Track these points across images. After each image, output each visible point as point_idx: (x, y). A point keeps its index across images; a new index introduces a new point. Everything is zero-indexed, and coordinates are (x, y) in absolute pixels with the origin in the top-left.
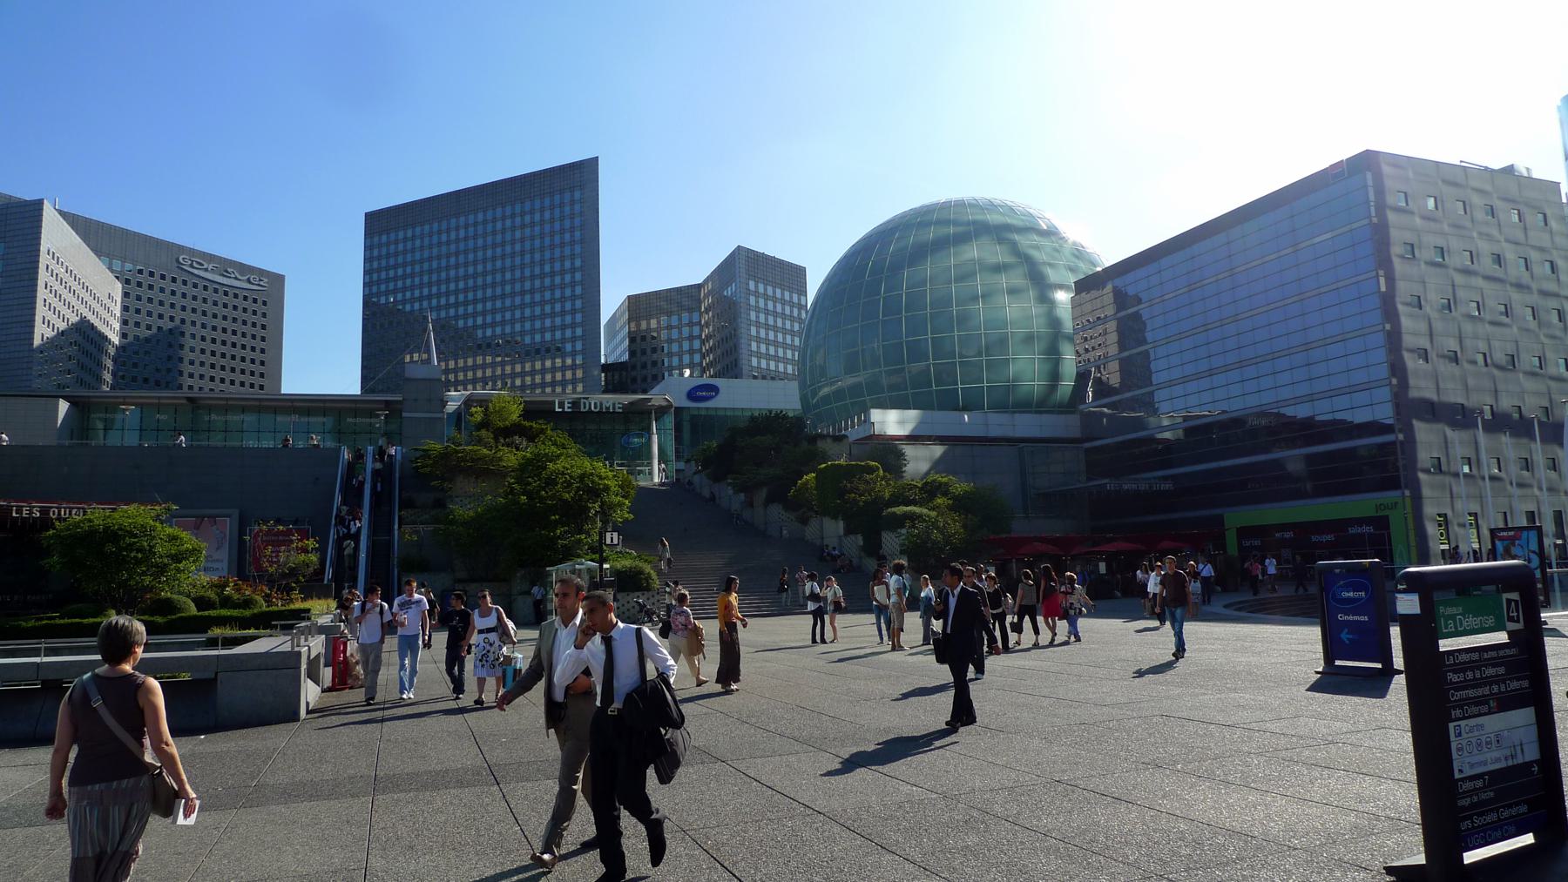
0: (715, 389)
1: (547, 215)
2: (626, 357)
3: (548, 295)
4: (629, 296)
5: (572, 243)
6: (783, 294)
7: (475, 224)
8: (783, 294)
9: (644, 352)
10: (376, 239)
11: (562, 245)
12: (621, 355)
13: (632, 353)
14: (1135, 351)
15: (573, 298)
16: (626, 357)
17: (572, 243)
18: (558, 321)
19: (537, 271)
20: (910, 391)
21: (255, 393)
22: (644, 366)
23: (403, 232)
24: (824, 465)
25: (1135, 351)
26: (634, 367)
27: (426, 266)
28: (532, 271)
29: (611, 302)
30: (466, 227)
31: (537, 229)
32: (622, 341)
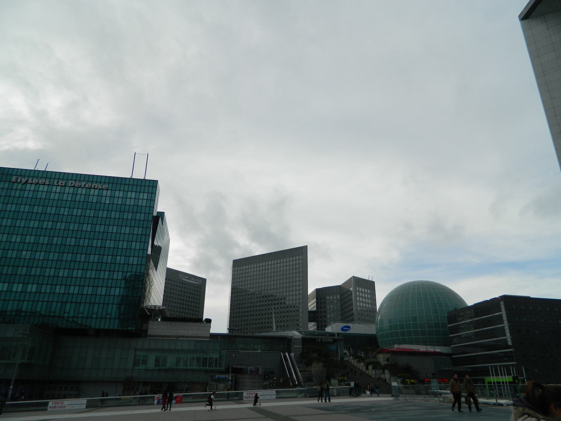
0: (349, 327)
1: (291, 263)
2: (315, 309)
3: (285, 290)
4: (317, 289)
5: (299, 272)
6: (367, 291)
7: (296, 260)
8: (367, 291)
9: (321, 308)
10: (236, 269)
11: (296, 273)
12: (313, 308)
13: (317, 308)
14: (462, 333)
15: (299, 290)
16: (315, 309)
17: (299, 272)
18: (298, 297)
19: (288, 281)
20: (433, 322)
21: (196, 317)
22: (321, 312)
23: (270, 262)
24: (296, 382)
25: (462, 333)
26: (318, 313)
27: (252, 278)
28: (299, 279)
29: (311, 289)
30: (293, 261)
31: (288, 267)
32: (313, 304)
